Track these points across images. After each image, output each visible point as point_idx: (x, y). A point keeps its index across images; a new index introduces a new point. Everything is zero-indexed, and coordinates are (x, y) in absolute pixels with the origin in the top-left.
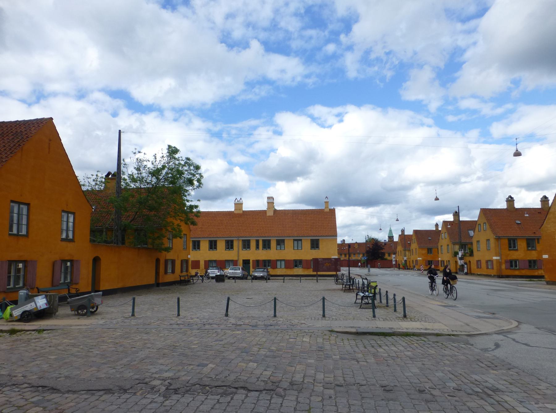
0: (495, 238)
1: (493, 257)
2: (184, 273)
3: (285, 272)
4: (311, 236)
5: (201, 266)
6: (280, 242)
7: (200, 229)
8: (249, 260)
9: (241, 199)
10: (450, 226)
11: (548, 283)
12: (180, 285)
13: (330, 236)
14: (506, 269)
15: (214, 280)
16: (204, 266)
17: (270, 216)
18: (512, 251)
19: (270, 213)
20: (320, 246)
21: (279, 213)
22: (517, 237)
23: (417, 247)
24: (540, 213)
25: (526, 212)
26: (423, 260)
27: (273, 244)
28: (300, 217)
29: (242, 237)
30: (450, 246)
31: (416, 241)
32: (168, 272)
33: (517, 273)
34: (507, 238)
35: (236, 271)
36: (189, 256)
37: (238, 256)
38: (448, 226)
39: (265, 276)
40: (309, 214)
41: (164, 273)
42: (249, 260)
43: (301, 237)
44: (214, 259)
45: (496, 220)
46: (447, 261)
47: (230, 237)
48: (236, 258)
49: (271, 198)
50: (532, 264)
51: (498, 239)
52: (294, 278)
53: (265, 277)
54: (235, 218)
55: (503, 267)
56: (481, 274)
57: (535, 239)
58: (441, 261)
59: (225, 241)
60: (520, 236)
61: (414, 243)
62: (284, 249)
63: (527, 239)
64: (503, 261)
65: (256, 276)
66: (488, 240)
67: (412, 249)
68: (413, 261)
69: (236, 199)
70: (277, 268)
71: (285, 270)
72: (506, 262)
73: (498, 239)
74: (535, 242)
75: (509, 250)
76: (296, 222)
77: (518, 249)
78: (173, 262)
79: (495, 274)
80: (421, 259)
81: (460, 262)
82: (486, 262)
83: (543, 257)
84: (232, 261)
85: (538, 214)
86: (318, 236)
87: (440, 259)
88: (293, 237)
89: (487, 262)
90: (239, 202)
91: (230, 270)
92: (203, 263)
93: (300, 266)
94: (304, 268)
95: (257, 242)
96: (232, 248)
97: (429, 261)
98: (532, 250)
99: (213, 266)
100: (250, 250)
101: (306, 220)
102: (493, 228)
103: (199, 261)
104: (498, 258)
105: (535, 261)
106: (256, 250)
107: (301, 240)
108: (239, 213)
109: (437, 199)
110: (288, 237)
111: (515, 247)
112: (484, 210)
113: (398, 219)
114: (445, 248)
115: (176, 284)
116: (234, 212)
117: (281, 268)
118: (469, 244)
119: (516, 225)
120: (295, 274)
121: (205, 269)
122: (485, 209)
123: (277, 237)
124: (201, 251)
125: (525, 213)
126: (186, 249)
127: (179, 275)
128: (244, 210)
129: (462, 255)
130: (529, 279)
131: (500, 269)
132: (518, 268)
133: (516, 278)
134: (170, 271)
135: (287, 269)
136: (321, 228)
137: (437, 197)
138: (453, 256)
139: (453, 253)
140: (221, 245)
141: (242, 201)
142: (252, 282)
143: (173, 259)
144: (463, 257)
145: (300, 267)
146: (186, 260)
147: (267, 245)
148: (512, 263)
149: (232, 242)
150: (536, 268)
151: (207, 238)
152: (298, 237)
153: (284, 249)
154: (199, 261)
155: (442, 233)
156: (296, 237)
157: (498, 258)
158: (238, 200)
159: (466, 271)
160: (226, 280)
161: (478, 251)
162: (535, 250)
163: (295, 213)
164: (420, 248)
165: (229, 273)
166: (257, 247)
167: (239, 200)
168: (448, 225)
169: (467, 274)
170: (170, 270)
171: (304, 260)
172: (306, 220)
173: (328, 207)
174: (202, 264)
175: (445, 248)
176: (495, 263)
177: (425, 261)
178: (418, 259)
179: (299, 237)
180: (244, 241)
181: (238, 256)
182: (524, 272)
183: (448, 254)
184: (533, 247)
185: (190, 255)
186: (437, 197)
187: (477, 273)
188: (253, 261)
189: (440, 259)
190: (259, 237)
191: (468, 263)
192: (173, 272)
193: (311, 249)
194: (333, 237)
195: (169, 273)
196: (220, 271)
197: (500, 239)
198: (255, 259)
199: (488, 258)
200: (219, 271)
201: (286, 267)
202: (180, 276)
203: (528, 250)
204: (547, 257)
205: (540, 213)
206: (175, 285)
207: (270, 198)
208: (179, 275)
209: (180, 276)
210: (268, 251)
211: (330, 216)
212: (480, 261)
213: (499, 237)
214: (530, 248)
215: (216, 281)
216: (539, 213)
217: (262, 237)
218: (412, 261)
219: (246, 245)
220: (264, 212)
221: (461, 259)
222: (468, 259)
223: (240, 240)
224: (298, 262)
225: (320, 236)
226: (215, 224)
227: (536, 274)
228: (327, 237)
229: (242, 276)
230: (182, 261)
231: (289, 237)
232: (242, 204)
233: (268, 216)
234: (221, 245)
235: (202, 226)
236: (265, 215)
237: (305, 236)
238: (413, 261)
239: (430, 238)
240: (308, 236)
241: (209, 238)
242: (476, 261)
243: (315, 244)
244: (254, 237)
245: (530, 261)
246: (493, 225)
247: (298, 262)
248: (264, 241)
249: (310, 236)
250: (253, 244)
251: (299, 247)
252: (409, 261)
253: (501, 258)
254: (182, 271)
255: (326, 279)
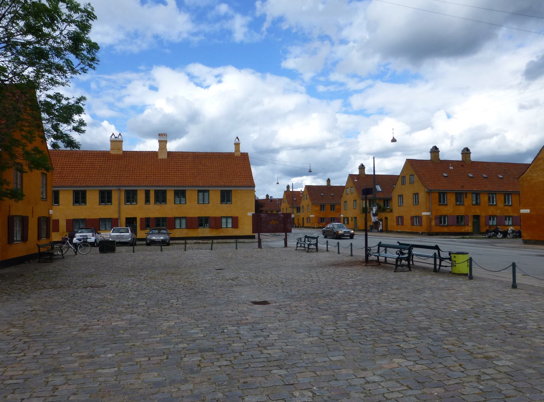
0: (427, 192)
1: (423, 213)
2: (44, 241)
3: (187, 233)
4: (222, 187)
5: (60, 228)
6: (180, 194)
7: (59, 175)
8: (136, 218)
9: (120, 134)
10: (356, 180)
11: (526, 242)
12: (39, 262)
13: (246, 186)
14: (436, 225)
15: (97, 249)
16: (65, 228)
17: (163, 160)
18: (442, 207)
19: (164, 156)
20: (233, 199)
21: (175, 155)
22: (444, 190)
23: (310, 204)
24: (463, 166)
25: (450, 165)
26: (316, 217)
27: (170, 196)
28: (203, 162)
29: (125, 186)
30: (358, 202)
31: (308, 196)
32: (15, 239)
33: (446, 230)
34: (437, 192)
35: (122, 234)
36: (51, 212)
37: (119, 213)
38: (355, 180)
39: (167, 240)
40: (216, 158)
41: (7, 241)
42: (136, 218)
43: (209, 187)
44: (82, 218)
45: (424, 172)
46: (352, 218)
47: (108, 187)
48: (115, 216)
49: (164, 135)
50: (460, 220)
51: (429, 192)
52: (201, 241)
53: (168, 241)
54: (113, 160)
55: (433, 223)
56: (403, 231)
57: (463, 193)
58: (344, 218)
59: (98, 192)
60: (450, 189)
61: (305, 199)
62: (186, 203)
63: (456, 193)
64: (433, 217)
65: (154, 240)
66: (416, 195)
67: (303, 206)
68: (303, 218)
69: (113, 134)
70: (175, 228)
71: (186, 231)
72: (436, 218)
73: (429, 192)
74: (463, 197)
75: (439, 205)
76: (200, 168)
77: (448, 204)
78: (24, 220)
79: (424, 231)
80: (314, 216)
81: (374, 219)
82: (411, 218)
83: (521, 212)
84: (110, 220)
85: (461, 167)
86: (231, 187)
87: (342, 216)
88: (197, 186)
89: (307, 218)
90: (116, 139)
91: (112, 233)
92: (65, 224)
93: (207, 225)
94: (211, 228)
95: (147, 193)
96: (109, 201)
97: (321, 218)
98: (460, 205)
99: (81, 227)
100: (137, 204)
101: (212, 166)
102: (423, 181)
103: (58, 220)
104: (429, 213)
105: (462, 217)
106: (145, 204)
107: (208, 191)
108: (117, 154)
109: (394, 140)
110: (190, 186)
111: (444, 202)
112: (410, 160)
113: (311, 170)
114: (350, 204)
115: (31, 261)
116: (110, 152)
117: (180, 228)
118: (498, 193)
119: (444, 178)
120: (199, 236)
121: (67, 231)
122: (411, 159)
123: (176, 186)
124: (60, 207)
125: (449, 166)
126: (46, 199)
127: (37, 245)
128: (124, 150)
129: (376, 211)
130: (462, 237)
131: (430, 226)
132: (446, 224)
133: (445, 235)
134: (19, 238)
135: (189, 230)
136: (233, 176)
137: (394, 138)
138: (362, 212)
139: (362, 209)
140: (93, 197)
141: (122, 138)
142: (161, 250)
143: (24, 215)
144: (377, 213)
145: (207, 226)
146: (46, 217)
147: (161, 197)
148: (440, 219)
149: (110, 193)
150: (463, 224)
151: (71, 187)
152: (204, 186)
153: (186, 203)
154: (58, 220)
155: (347, 188)
156: (202, 187)
157: (429, 213)
158: (116, 136)
159: (380, 228)
160: (118, 249)
161: (399, 206)
162: (463, 205)
163: (196, 156)
164: (313, 204)
165: (111, 236)
166: (147, 200)
167: (117, 136)
168: (354, 179)
169: (382, 231)
170: (18, 236)
171: (152, 218)
172: (212, 166)
173: (239, 151)
174: (63, 225)
175: (350, 204)
176: (424, 219)
177: (317, 219)
178: (311, 216)
179: (206, 187)
180: (127, 192)
181: (119, 213)
182: (453, 229)
183: (355, 210)
184: (461, 202)
185: (52, 209)
186: (394, 138)
187: (396, 230)
188: (141, 219)
189: (342, 216)
190: (150, 187)
191: (384, 220)
192: (24, 238)
193: (221, 204)
194: (250, 187)
195: (17, 241)
196: (95, 234)
197: (432, 192)
198: (144, 216)
199: (413, 214)
200: (94, 235)
201: (188, 227)
202: (39, 247)
203: (456, 205)
204: (529, 212)
205: (463, 166)
206: (30, 263)
207: (162, 135)
208: (37, 245)
209: (39, 247)
210: (164, 205)
211: (243, 162)
212: (402, 217)
213: (430, 190)
214: (458, 203)
215: (100, 251)
216: (461, 166)
217: (155, 186)
218: (302, 219)
219: (131, 197)
220: (154, 154)
221: (375, 215)
222: (383, 215)
223: (122, 190)
224: (161, 220)
225: (233, 187)
226: (82, 168)
227: (463, 231)
228: (246, 187)
229: (132, 240)
230: (39, 219)
231: (193, 186)
232: (122, 141)
233: (160, 160)
234: (93, 197)
235: (61, 170)
236: (155, 157)
237: (213, 186)
238: (303, 218)
239: (322, 194)
240: (217, 186)
241: (74, 187)
242: (396, 217)
243: (226, 197)
244: (143, 186)
245: (458, 217)
246: (422, 177)
247: (161, 220)
248: (156, 192)
249: (220, 186)
250: (141, 196)
251: (205, 200)
252: (298, 219)
253: (432, 214)
254: (39, 238)
255: (253, 242)
